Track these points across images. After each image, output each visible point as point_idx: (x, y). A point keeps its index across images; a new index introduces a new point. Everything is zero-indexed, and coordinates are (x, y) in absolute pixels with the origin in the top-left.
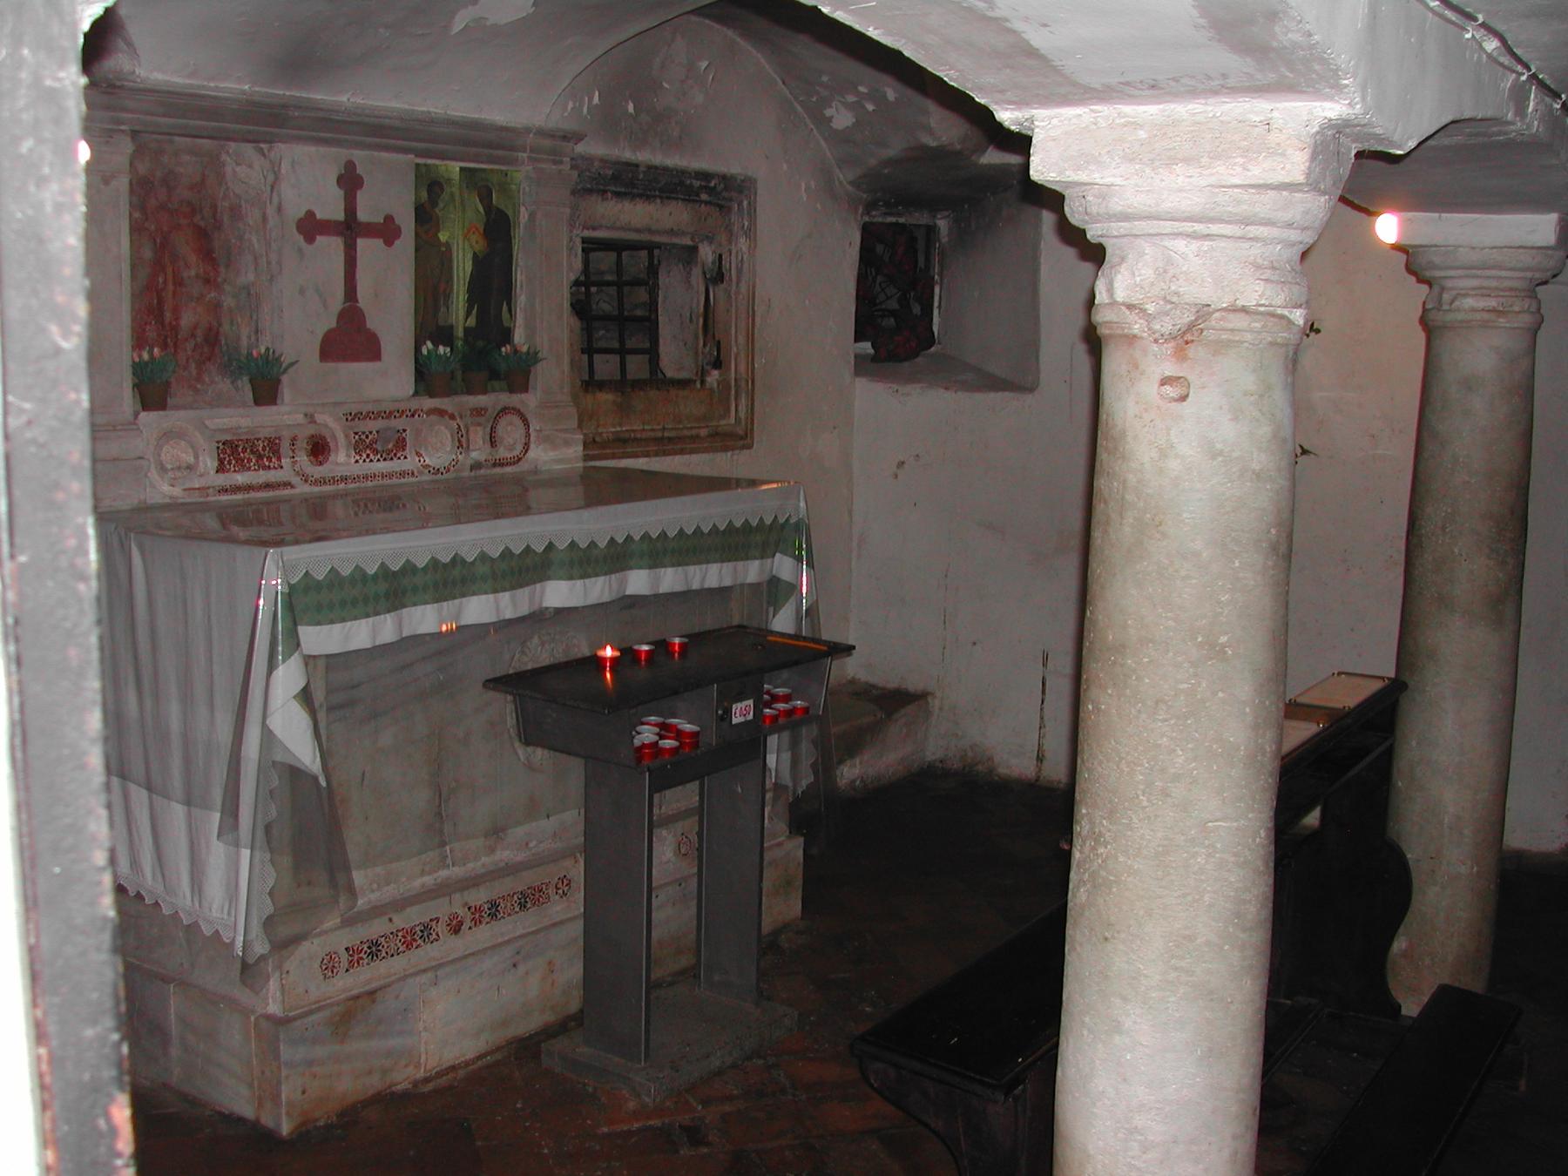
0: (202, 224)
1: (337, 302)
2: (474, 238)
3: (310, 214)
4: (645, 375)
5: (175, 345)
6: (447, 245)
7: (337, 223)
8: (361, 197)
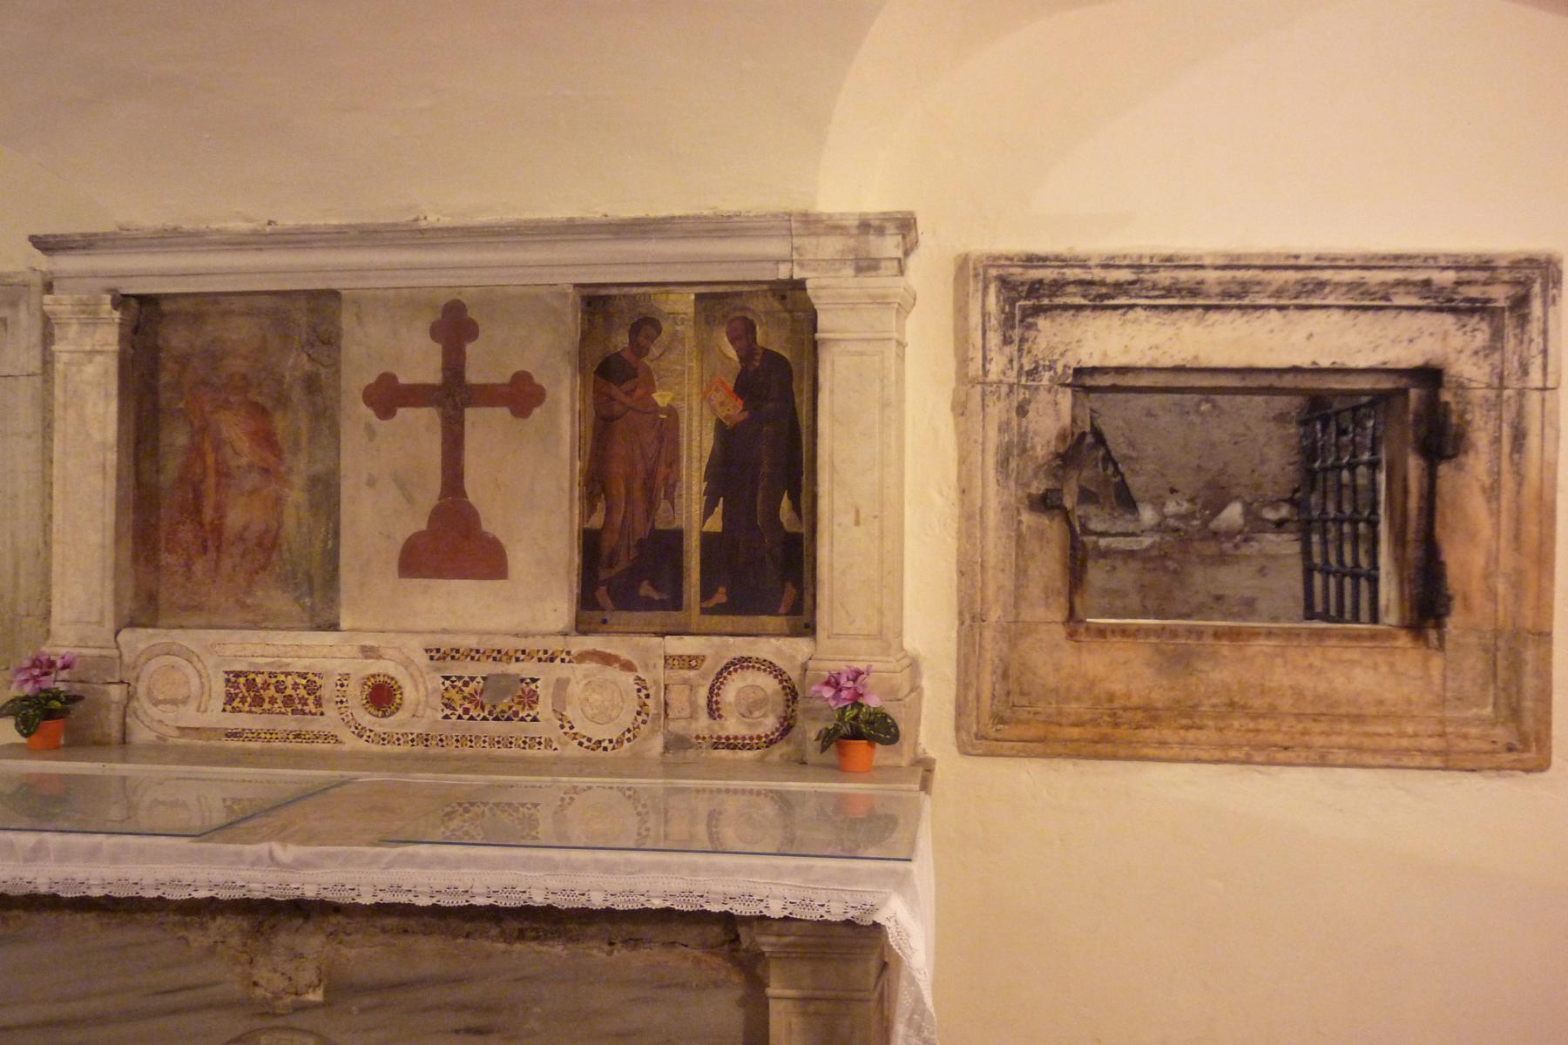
0: (260, 399)
2: (718, 397)
3: (387, 380)
5: (218, 548)
6: (672, 412)
7: (432, 387)
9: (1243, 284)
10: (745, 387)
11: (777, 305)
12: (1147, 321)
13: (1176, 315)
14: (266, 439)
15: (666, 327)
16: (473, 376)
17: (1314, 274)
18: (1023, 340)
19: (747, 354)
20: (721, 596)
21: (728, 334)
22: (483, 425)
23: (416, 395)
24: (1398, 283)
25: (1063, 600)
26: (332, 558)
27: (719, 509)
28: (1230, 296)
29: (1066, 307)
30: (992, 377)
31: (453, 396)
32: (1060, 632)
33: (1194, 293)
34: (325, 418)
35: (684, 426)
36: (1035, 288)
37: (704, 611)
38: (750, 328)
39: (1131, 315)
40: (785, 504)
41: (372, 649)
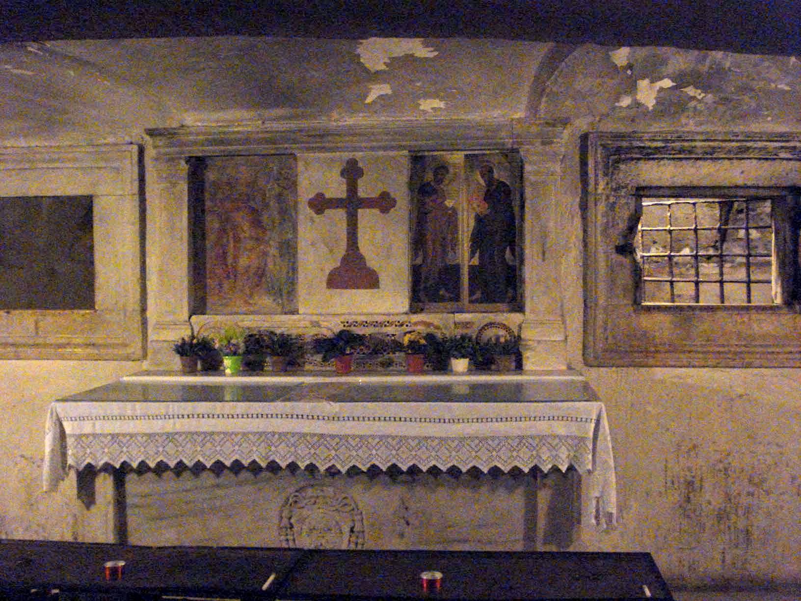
1: (342, 249)
3: (320, 196)
4: (715, 302)
8: (361, 183)
9: (714, 148)
10: (489, 196)
11: (503, 160)
12: (669, 165)
13: (684, 162)
14: (257, 223)
15: (451, 170)
16: (362, 194)
17: (745, 144)
18: (613, 174)
19: (490, 182)
20: (478, 295)
21: (481, 173)
22: (367, 217)
23: (335, 203)
24: (782, 147)
25: (631, 295)
26: (292, 282)
27: (477, 255)
28: (707, 154)
29: (632, 159)
30: (599, 191)
31: (352, 204)
32: (630, 309)
33: (690, 152)
34: (288, 215)
35: (460, 217)
36: (618, 150)
37: (471, 302)
38: (491, 171)
39: (662, 162)
40: (508, 251)
41: (317, 322)
